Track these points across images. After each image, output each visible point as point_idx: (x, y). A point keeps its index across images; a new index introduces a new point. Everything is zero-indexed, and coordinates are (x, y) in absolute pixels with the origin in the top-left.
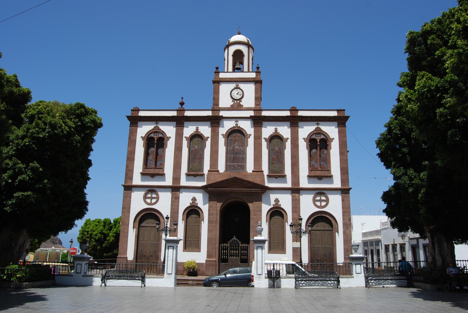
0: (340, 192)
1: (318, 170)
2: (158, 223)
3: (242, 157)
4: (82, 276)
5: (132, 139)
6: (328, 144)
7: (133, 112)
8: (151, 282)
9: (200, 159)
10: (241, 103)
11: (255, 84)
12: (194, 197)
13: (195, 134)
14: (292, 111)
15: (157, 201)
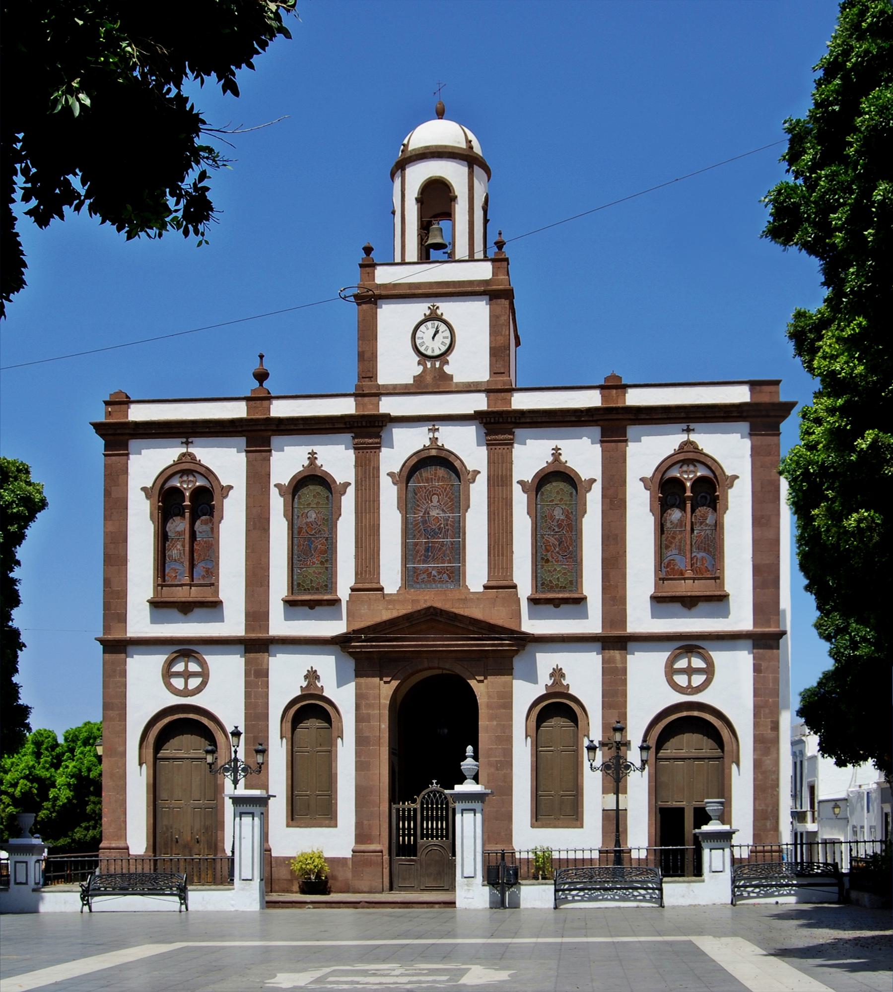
0: (749, 643)
1: (685, 579)
2: (210, 748)
3: (452, 544)
4: (31, 890)
6: (717, 494)
7: (110, 409)
9: (326, 552)
10: (446, 369)
11: (490, 300)
12: (312, 668)
14: (606, 391)
15: (204, 684)
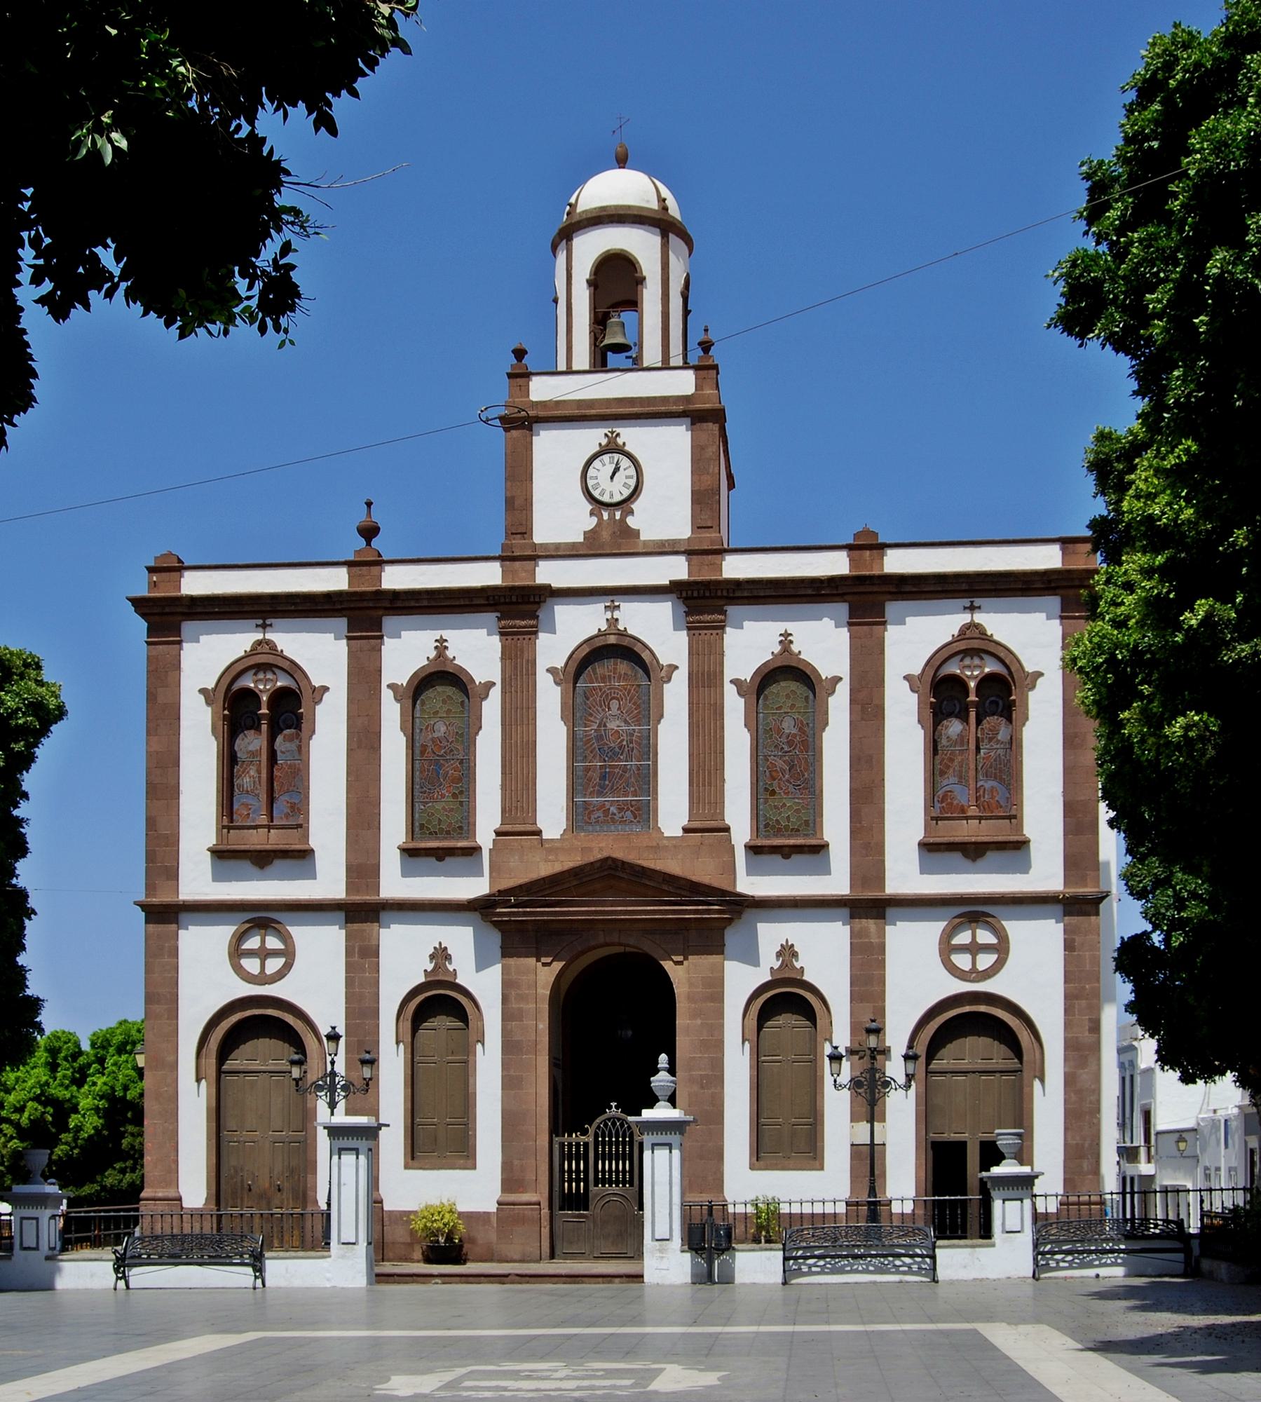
1: (967, 818)
2: (296, 1057)
3: (639, 769)
5: (161, 700)
6: (1013, 698)
7: (155, 579)
9: (460, 780)
10: (630, 521)
11: (693, 424)
12: (440, 944)
15: (288, 967)
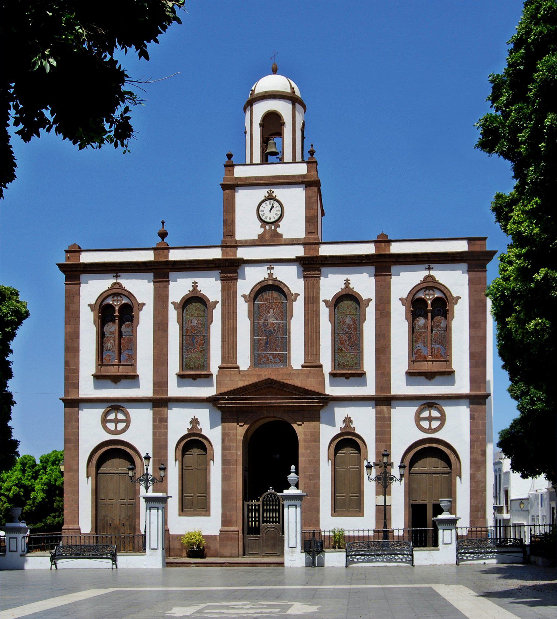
0: (467, 401)
1: (427, 361)
2: (131, 467)
5: (71, 309)
6: (447, 308)
7: (68, 256)
8: (127, 562)
9: (203, 344)
10: (278, 230)
11: (306, 187)
12: (194, 417)
13: (191, 296)
14: (378, 244)
15: (127, 427)
